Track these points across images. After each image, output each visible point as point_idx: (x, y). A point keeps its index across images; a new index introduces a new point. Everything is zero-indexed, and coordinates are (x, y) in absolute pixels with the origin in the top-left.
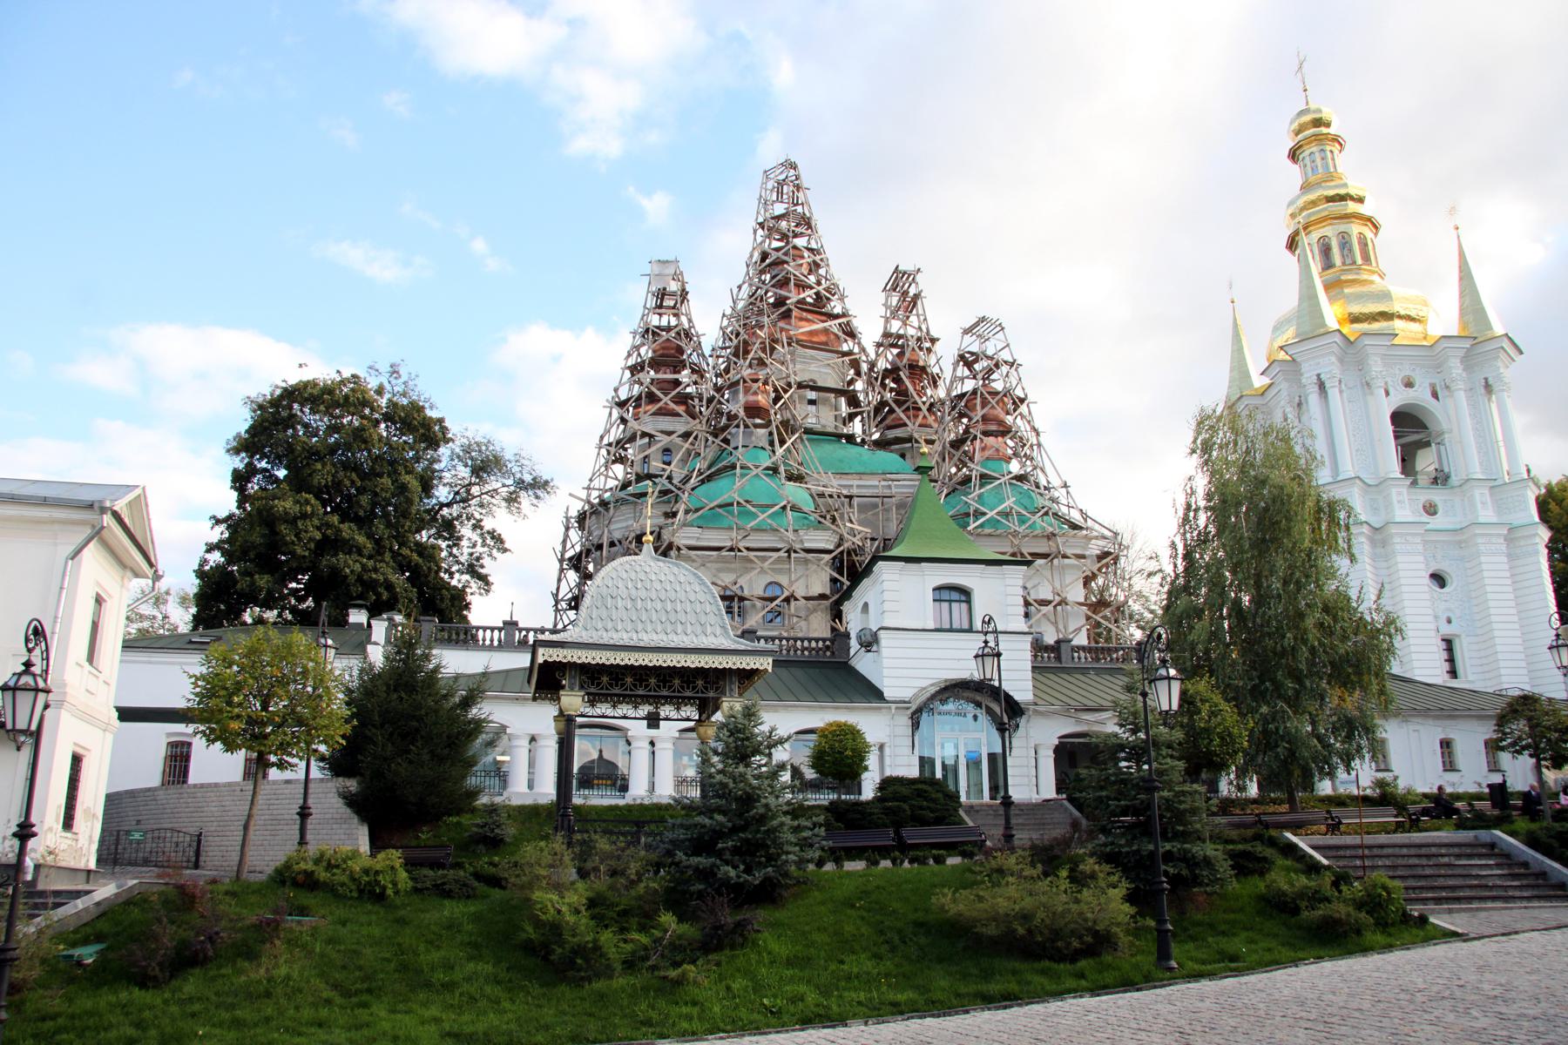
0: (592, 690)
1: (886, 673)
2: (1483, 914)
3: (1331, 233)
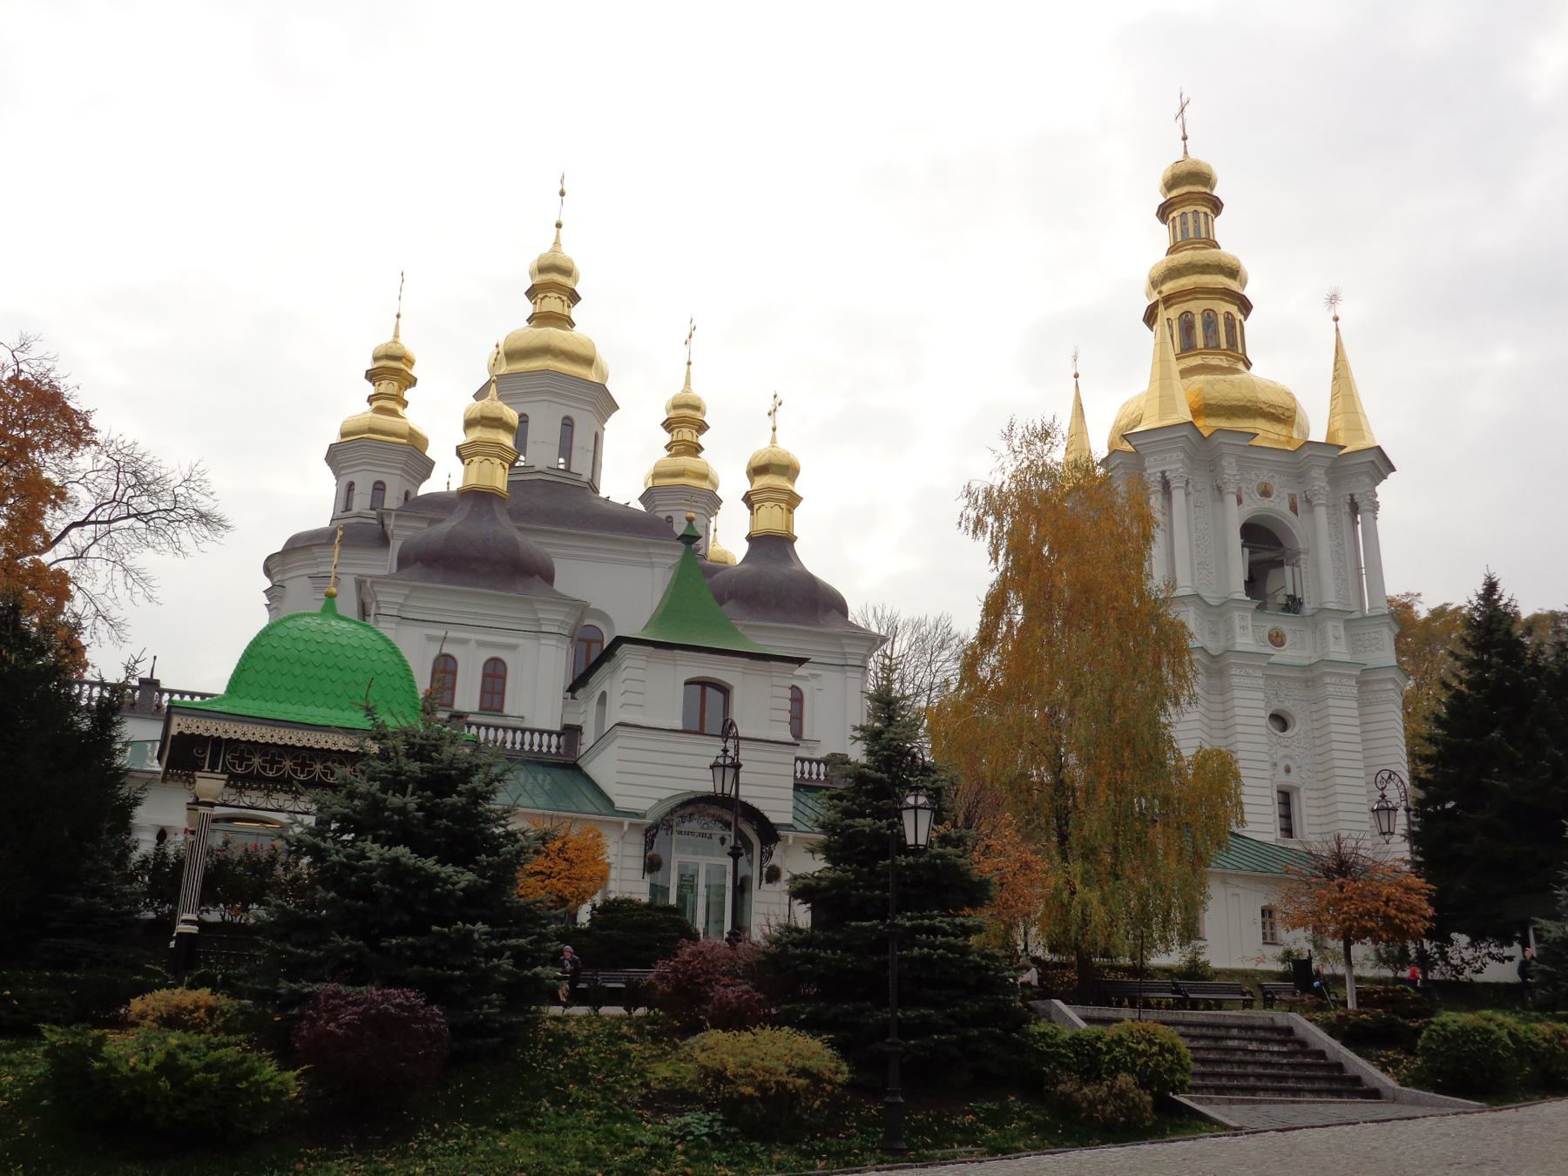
2: (1264, 1108)
3: (1200, 305)
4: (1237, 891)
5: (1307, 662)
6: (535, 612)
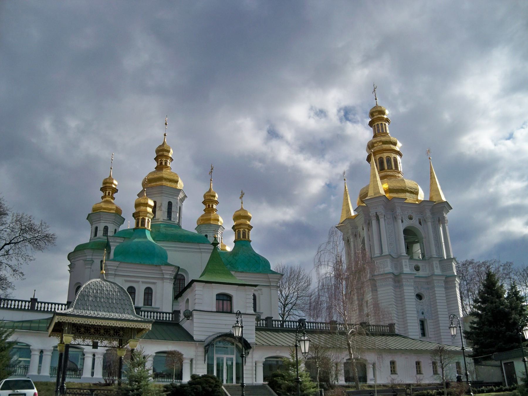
6: (162, 270)
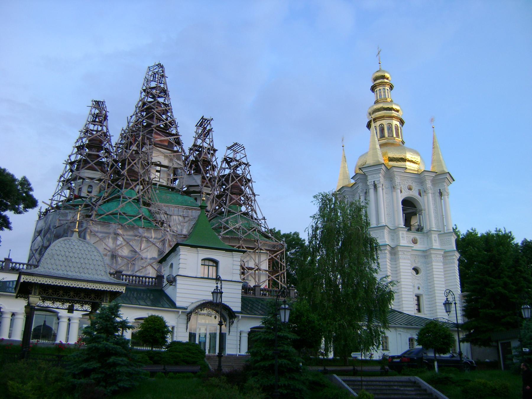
0: (44, 295)
1: (178, 295)
4: (400, 332)
5: (425, 249)
